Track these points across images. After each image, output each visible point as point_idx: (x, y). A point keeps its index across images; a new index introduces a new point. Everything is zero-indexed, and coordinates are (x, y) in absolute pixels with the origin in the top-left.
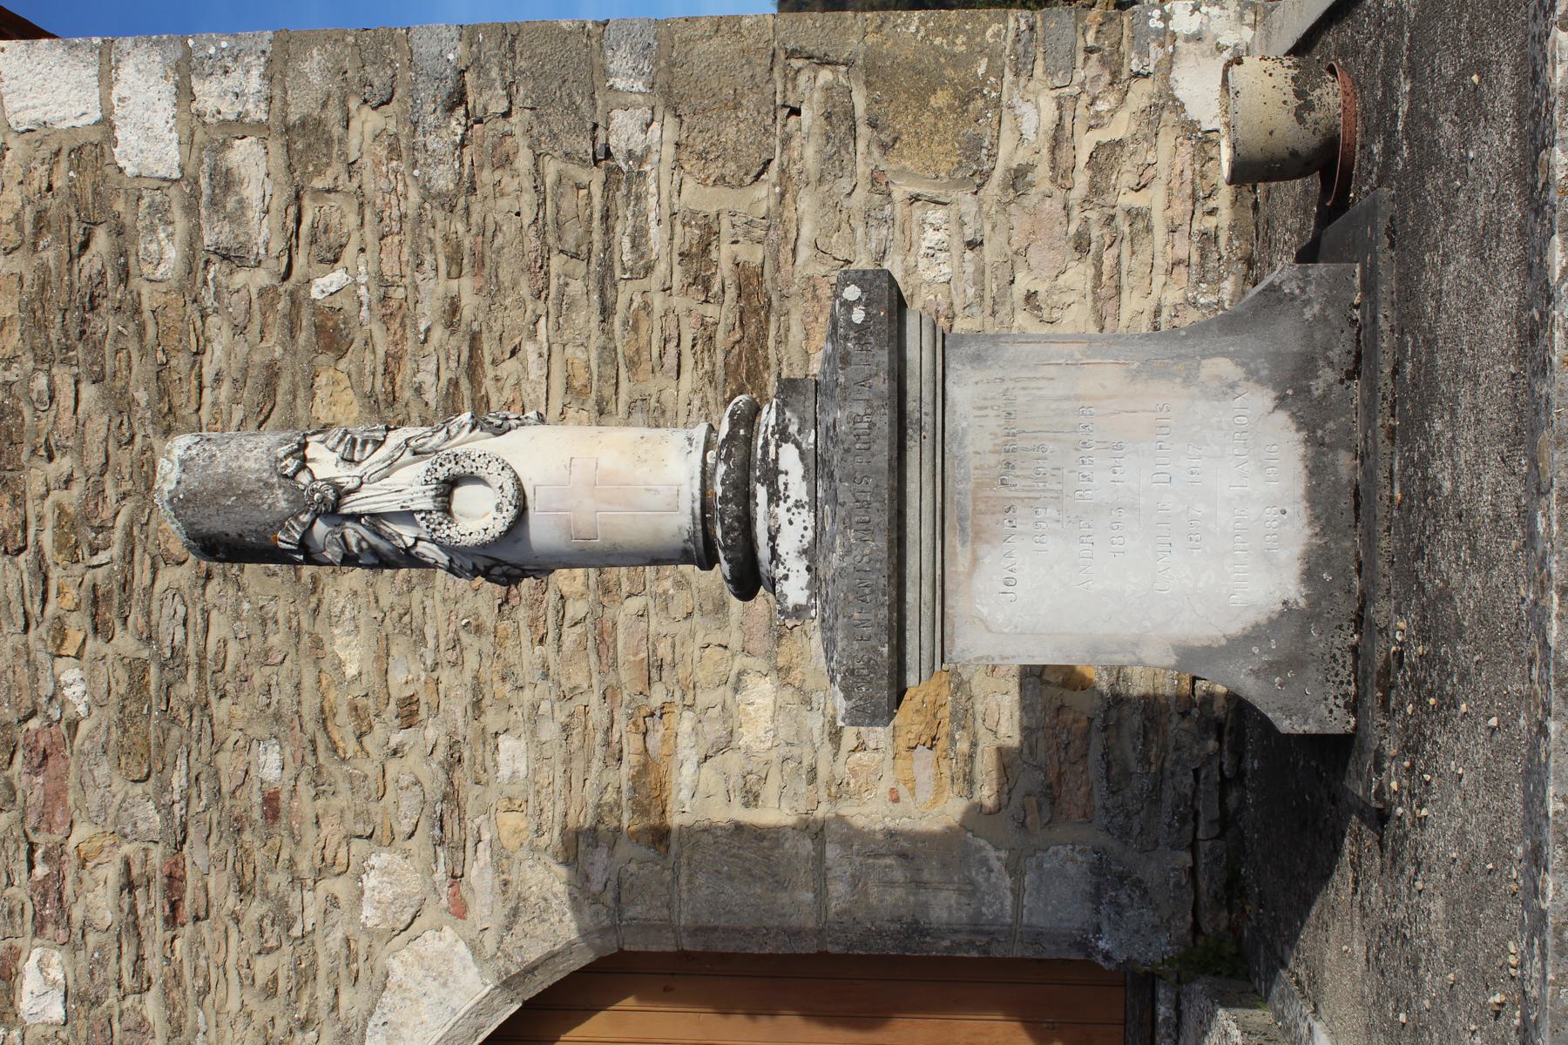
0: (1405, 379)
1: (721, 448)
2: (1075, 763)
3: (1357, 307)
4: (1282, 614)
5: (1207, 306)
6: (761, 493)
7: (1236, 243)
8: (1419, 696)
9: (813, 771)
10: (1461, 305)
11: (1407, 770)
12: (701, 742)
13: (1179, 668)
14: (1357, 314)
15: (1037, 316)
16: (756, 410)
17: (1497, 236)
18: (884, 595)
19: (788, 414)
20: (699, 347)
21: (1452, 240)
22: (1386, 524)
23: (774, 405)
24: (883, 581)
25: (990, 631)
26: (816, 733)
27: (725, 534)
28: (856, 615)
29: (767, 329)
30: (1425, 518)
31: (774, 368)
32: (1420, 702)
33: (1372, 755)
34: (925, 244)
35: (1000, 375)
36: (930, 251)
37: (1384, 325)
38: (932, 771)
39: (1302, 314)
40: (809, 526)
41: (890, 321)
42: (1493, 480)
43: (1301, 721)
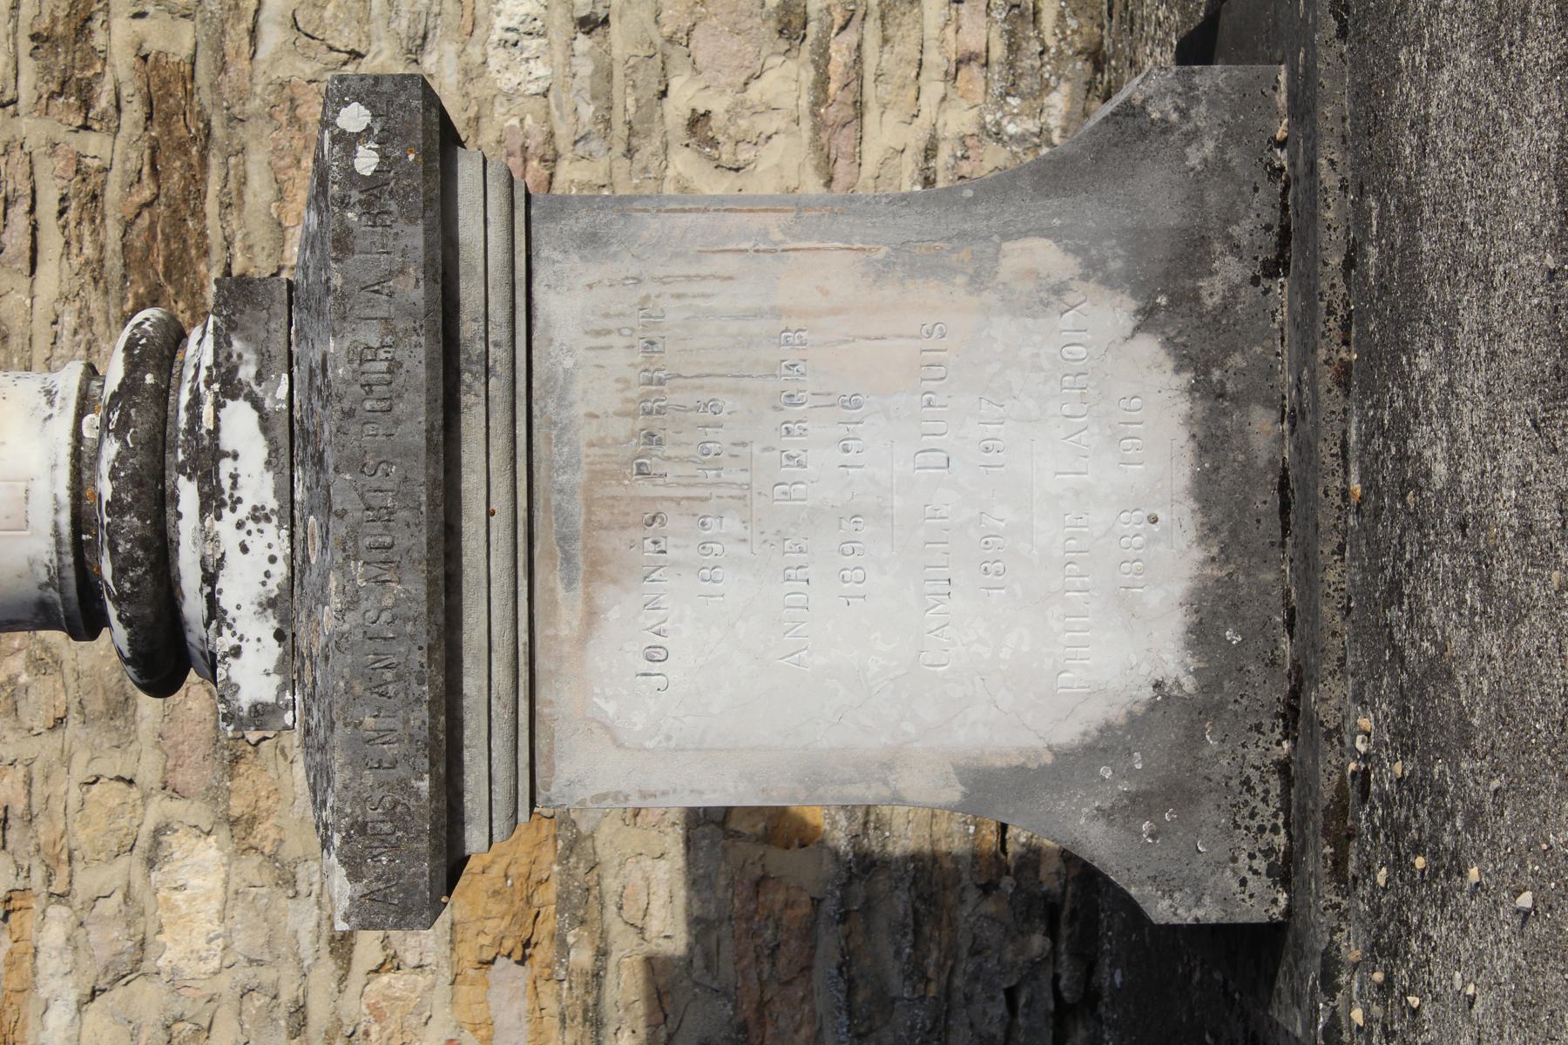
0: (1366, 277)
1: (110, 408)
2: (789, 983)
3: (1282, 144)
4: (1152, 706)
5: (1021, 139)
6: (188, 493)
7: (1072, 23)
8: (1398, 854)
9: (299, 1012)
10: (1461, 144)
11: (1380, 987)
12: (85, 963)
13: (970, 807)
14: (1282, 156)
15: (710, 158)
16: (177, 337)
17: (1523, 20)
18: (421, 683)
19: (237, 345)
20: (72, 215)
21: (1445, 25)
22: (1337, 539)
23: (210, 327)
24: (419, 657)
25: (619, 745)
26: (306, 939)
27: (119, 572)
28: (369, 721)
29: (204, 180)
30: (1403, 530)
31: (217, 254)
32: (1400, 864)
33: (1318, 960)
34: (501, 22)
35: (634, 271)
36: (512, 37)
37: (1329, 179)
38: (523, 1005)
39: (1183, 158)
40: (280, 556)
41: (427, 171)
42: (1519, 462)
43: (1191, 901)
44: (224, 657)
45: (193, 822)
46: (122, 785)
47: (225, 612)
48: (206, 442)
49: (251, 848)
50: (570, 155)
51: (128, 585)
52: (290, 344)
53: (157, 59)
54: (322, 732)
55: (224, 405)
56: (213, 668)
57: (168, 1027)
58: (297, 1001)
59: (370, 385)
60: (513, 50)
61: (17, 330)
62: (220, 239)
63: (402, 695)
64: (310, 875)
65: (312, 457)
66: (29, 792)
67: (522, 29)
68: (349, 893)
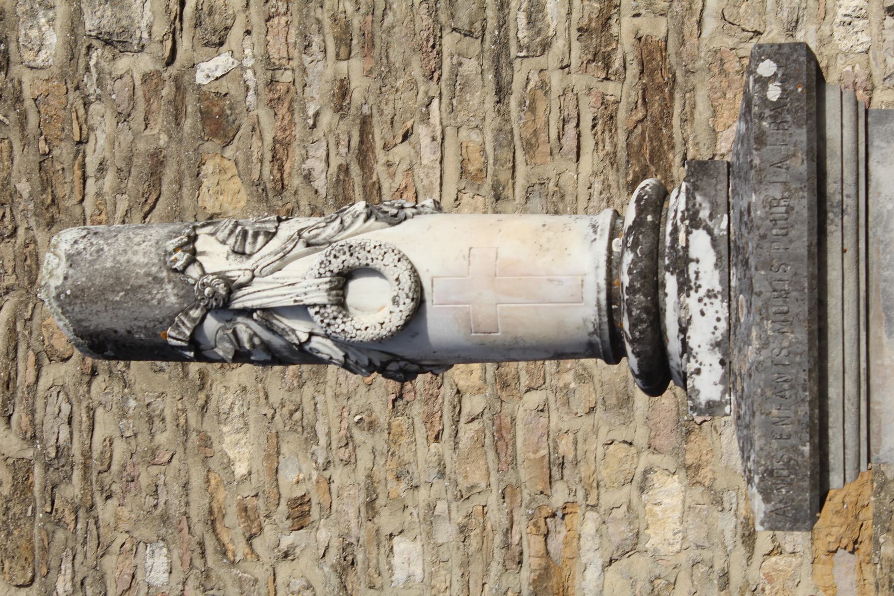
1: (628, 235)
6: (671, 282)
9: (725, 577)
16: (663, 194)
19: (699, 199)
20: (599, 128)
24: (804, 376)
26: (728, 535)
27: (633, 326)
28: (775, 412)
29: (672, 107)
31: (679, 148)
34: (841, 11)
36: (848, 19)
38: (853, 577)
40: (722, 317)
41: (809, 98)
44: (691, 374)
45: (665, 467)
46: (626, 446)
47: (692, 349)
48: (681, 253)
49: (697, 482)
50: (881, 87)
51: (637, 334)
52: (728, 197)
53: (646, 40)
54: (747, 418)
55: (691, 233)
56: (685, 380)
57: (652, 582)
58: (723, 570)
59: (775, 220)
60: (848, 27)
61: (569, 192)
62: (681, 139)
63: (793, 397)
64: (731, 499)
65: (742, 261)
66: (576, 449)
67: (854, 15)
68: (763, 509)
